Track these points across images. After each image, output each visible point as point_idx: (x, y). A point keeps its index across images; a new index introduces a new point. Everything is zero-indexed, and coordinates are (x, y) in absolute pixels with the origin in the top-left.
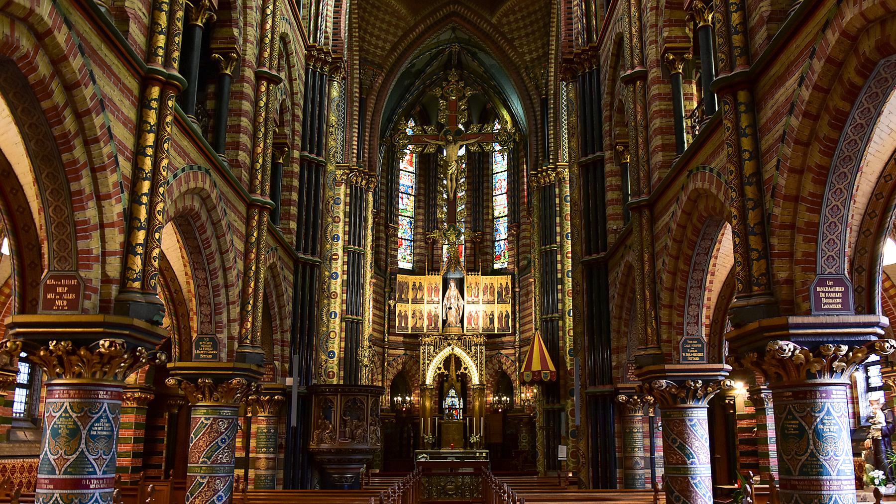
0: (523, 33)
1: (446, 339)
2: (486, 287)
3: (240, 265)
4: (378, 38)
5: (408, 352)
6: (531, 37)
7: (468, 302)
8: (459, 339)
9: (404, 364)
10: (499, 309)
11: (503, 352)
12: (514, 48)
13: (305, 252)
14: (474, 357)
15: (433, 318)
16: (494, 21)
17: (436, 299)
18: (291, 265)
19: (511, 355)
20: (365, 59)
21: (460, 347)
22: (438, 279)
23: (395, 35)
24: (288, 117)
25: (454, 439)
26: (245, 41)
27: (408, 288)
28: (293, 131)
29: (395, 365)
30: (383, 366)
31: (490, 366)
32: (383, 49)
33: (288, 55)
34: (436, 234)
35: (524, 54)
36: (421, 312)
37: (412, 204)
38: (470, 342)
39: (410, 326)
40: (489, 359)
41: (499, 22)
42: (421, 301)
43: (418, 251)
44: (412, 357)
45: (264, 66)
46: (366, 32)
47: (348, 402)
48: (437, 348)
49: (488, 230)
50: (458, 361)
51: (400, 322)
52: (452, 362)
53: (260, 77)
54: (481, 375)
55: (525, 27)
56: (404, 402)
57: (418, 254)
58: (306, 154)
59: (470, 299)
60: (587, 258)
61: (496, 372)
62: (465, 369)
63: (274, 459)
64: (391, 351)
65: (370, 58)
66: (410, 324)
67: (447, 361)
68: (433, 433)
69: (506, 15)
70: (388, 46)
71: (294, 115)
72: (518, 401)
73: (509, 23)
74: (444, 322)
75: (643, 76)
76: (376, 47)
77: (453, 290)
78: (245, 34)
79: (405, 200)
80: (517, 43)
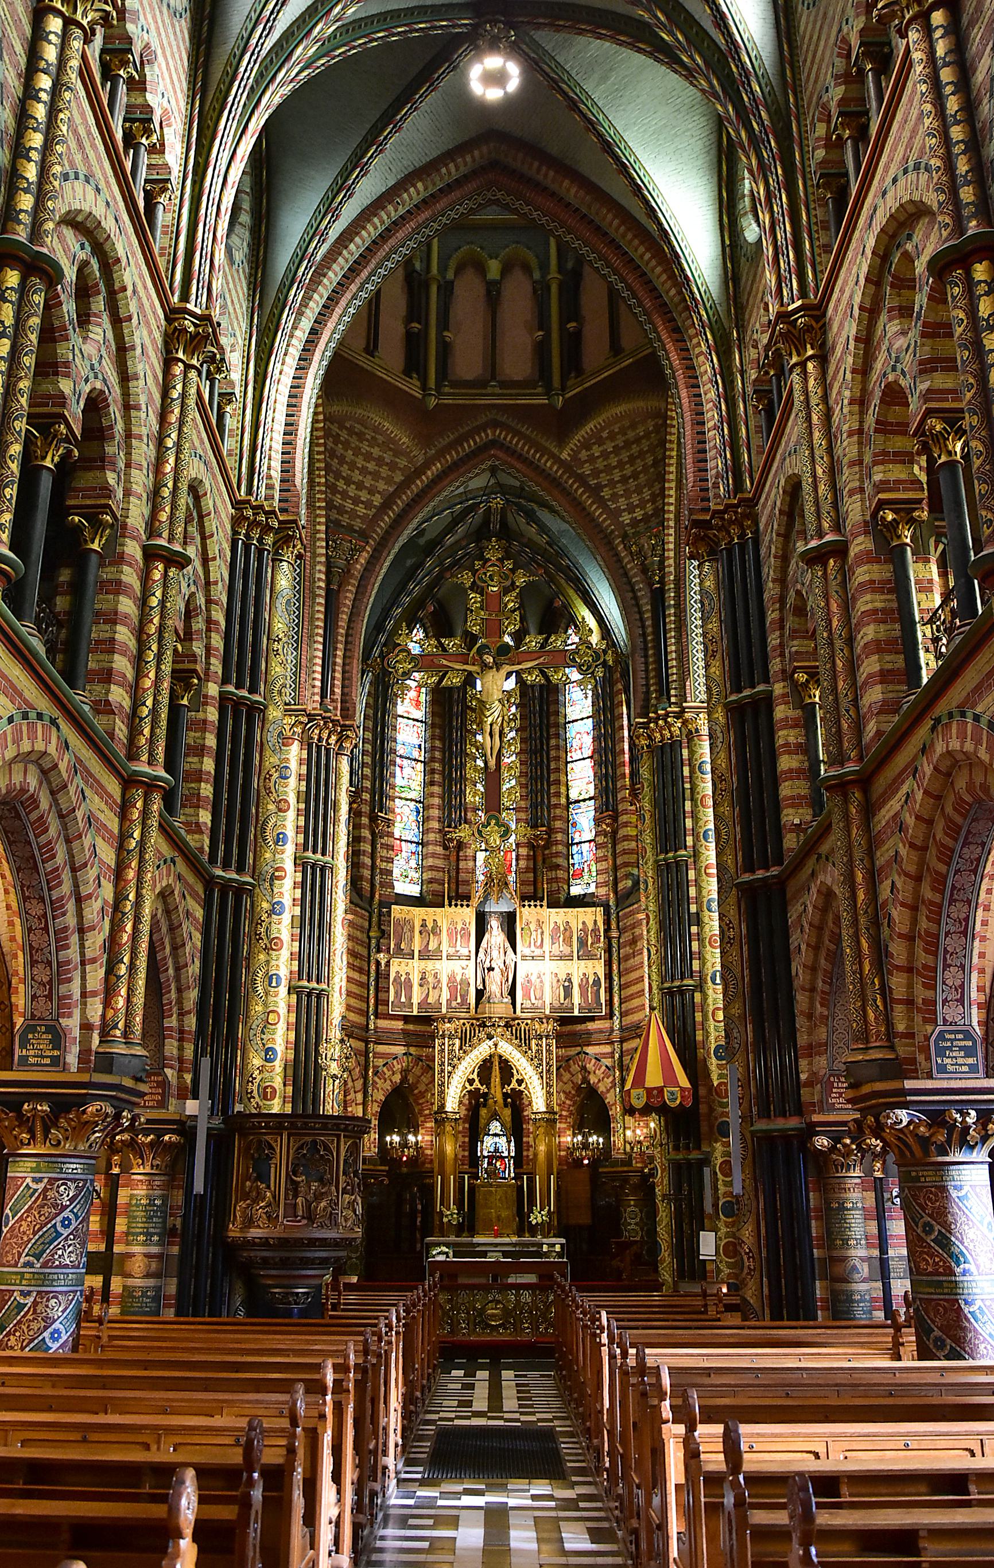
0: (617, 476)
1: (483, 1025)
3: (108, 891)
5: (412, 1050)
7: (524, 958)
8: (507, 1025)
9: (405, 1072)
11: (590, 1050)
13: (226, 866)
14: (536, 1060)
15: (457, 987)
16: (565, 455)
17: (464, 952)
18: (200, 889)
19: (605, 1055)
20: (337, 523)
22: (466, 915)
23: (389, 480)
24: (199, 624)
25: (499, 1218)
26: (128, 493)
28: (208, 648)
29: (388, 1073)
30: (365, 1077)
31: (566, 1076)
32: (368, 505)
33: (201, 517)
36: (435, 975)
37: (420, 777)
39: (416, 1000)
40: (564, 1064)
41: (575, 456)
43: (430, 862)
44: (419, 1059)
45: (160, 536)
46: (338, 476)
47: (301, 1147)
48: (467, 1040)
49: (558, 824)
50: (507, 1068)
51: (398, 995)
53: (151, 554)
54: (549, 1094)
55: (621, 465)
56: (404, 1144)
57: (431, 868)
58: (231, 688)
59: (527, 952)
60: (747, 877)
61: (579, 1089)
62: (520, 1082)
63: (159, 1257)
64: (381, 1049)
65: (345, 520)
67: (485, 1068)
68: (460, 1205)
69: (586, 445)
70: (377, 500)
71: (209, 621)
72: (619, 1144)
73: (592, 459)
74: (480, 994)
75: (840, 550)
77: (496, 935)
78: (128, 481)
79: (407, 771)
80: (606, 493)
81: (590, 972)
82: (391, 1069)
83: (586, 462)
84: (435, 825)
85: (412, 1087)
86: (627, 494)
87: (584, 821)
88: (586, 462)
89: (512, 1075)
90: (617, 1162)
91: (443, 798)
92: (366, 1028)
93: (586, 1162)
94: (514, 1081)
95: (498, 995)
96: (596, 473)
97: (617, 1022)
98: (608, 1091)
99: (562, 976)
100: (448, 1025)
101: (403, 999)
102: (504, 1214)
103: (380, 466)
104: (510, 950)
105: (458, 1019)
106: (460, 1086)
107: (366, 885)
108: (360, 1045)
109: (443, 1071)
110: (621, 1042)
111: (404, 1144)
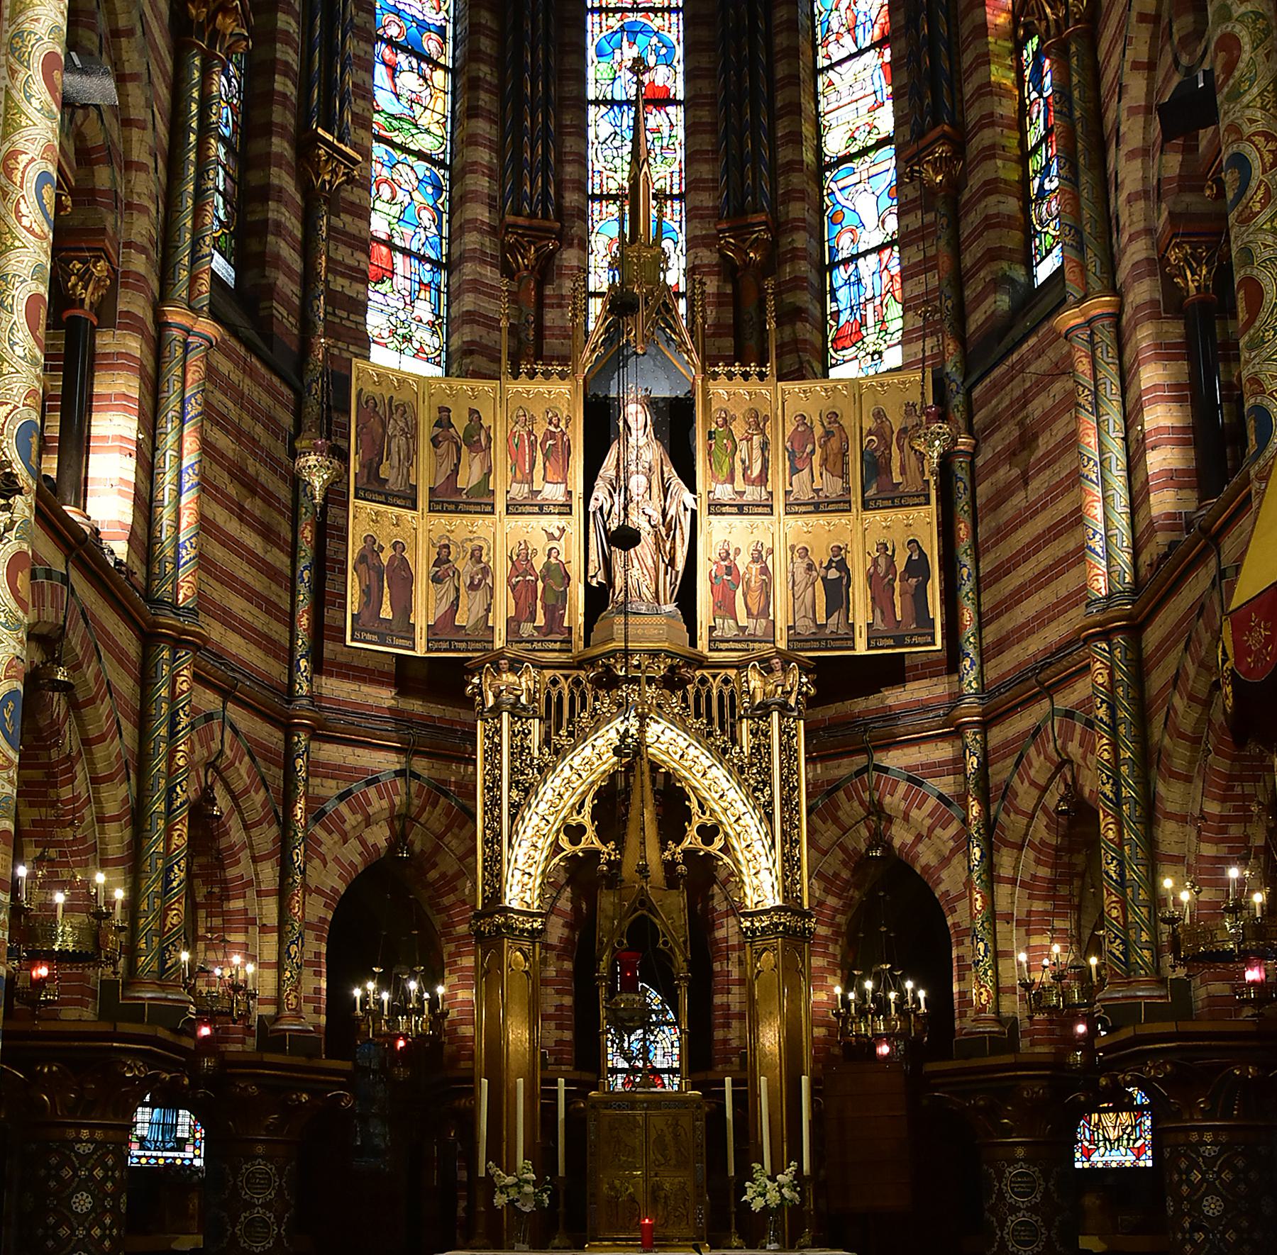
1: (608, 681)
2: (804, 432)
5: (420, 765)
7: (716, 508)
8: (672, 682)
9: (401, 821)
10: (865, 534)
11: (895, 759)
14: (752, 775)
15: (538, 585)
17: (553, 493)
19: (935, 769)
21: (679, 721)
22: (558, 397)
25: (655, 1193)
27: (411, 433)
29: (352, 820)
30: (286, 823)
31: (829, 833)
36: (476, 555)
37: (442, 104)
38: (729, 704)
39: (421, 619)
40: (825, 799)
42: (480, 500)
43: (469, 302)
44: (438, 789)
48: (562, 721)
49: (797, 210)
50: (673, 802)
51: (371, 597)
52: (638, 797)
54: (790, 864)
56: (400, 1007)
57: (470, 318)
59: (724, 492)
61: (860, 863)
62: (708, 833)
64: (331, 753)
66: (425, 608)
67: (610, 804)
68: (542, 1157)
72: (981, 995)
74: (597, 599)
77: (640, 443)
79: (409, 81)
81: (899, 539)
82: (360, 806)
84: (482, 213)
85: (422, 863)
87: (865, 206)
89: (688, 816)
90: (976, 1044)
91: (499, 150)
92: (289, 692)
93: (884, 1050)
94: (692, 831)
95: (648, 594)
97: (971, 676)
98: (945, 861)
99: (821, 556)
100: (508, 678)
101: (386, 613)
102: (670, 1183)
104: (677, 483)
105: (541, 667)
106: (544, 844)
107: (285, 319)
108: (269, 735)
109: (496, 802)
110: (985, 726)
111: (400, 1007)
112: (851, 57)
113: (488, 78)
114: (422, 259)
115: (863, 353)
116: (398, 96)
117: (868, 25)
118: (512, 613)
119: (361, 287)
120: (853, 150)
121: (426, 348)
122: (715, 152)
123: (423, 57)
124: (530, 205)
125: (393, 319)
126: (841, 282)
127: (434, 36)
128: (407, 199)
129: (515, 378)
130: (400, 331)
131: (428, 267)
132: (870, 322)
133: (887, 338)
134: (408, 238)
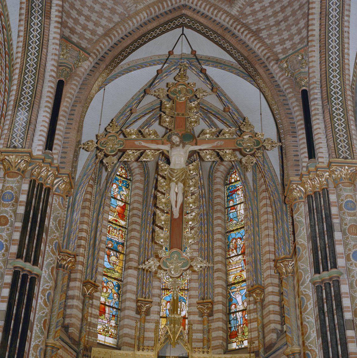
0: (272, 21)
4: (88, 18)
6: (283, 25)
12: (261, 40)
23: (110, 20)
32: (93, 33)
34: (152, 264)
35: (273, 45)
41: (242, 13)
55: (275, 14)
65: (75, 39)
70: (100, 31)
73: (254, 13)
76: (85, 28)
79: (113, 258)
80: (264, 34)
83: (249, 15)
86: (279, 32)
88: (249, 15)
96: (257, 22)
103: (104, 9)
112: (235, 256)
113: (135, 258)
114: (113, 308)
115: (237, 341)
116: (110, 263)
117: (240, 248)
118: (69, 6)
119: (96, 320)
120: (236, 281)
121: (113, 334)
122: (198, 280)
123: (117, 251)
124: (145, 294)
125: (104, 326)
126: (232, 319)
127: (121, 245)
128: (110, 292)
129: (139, 351)
130: (106, 330)
131: (115, 310)
132: (240, 331)
133: (245, 337)
134: (110, 302)
